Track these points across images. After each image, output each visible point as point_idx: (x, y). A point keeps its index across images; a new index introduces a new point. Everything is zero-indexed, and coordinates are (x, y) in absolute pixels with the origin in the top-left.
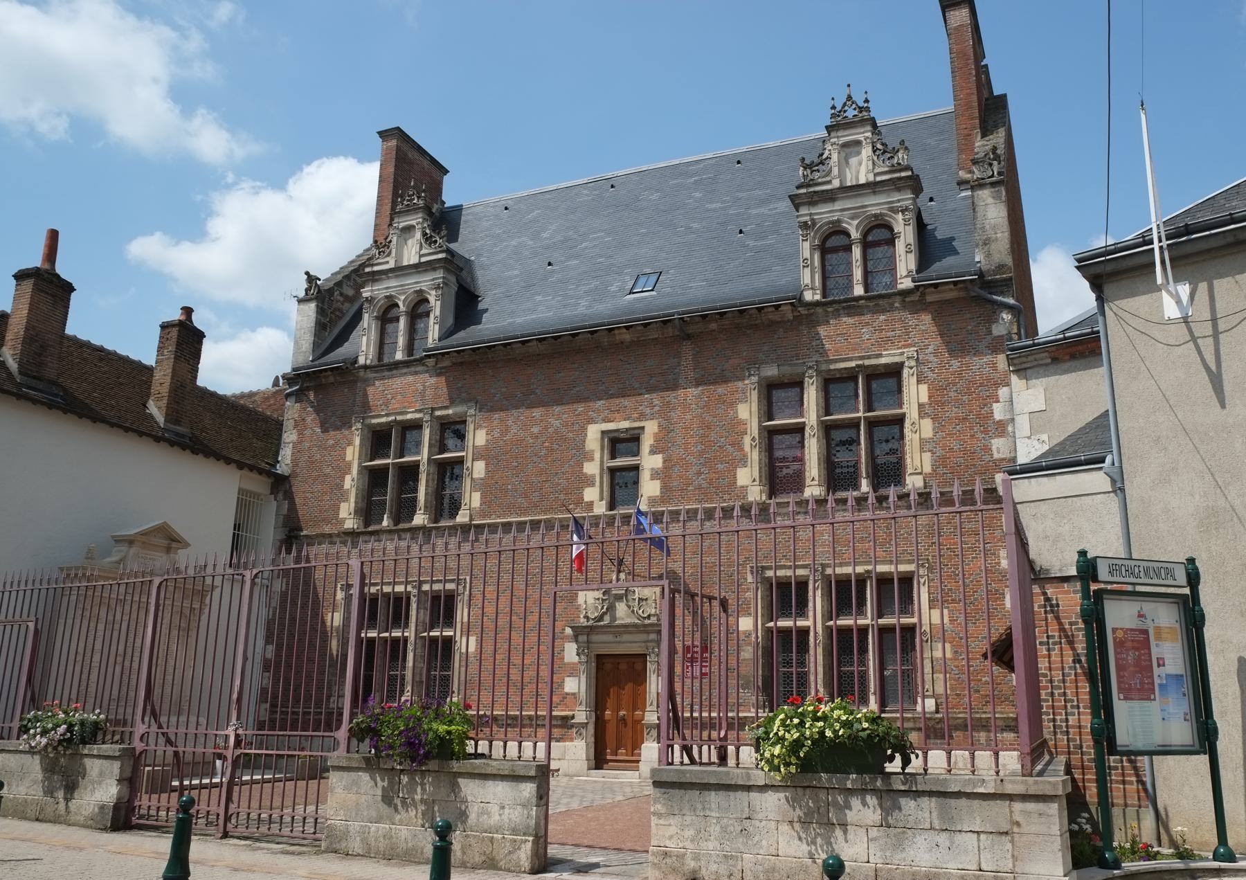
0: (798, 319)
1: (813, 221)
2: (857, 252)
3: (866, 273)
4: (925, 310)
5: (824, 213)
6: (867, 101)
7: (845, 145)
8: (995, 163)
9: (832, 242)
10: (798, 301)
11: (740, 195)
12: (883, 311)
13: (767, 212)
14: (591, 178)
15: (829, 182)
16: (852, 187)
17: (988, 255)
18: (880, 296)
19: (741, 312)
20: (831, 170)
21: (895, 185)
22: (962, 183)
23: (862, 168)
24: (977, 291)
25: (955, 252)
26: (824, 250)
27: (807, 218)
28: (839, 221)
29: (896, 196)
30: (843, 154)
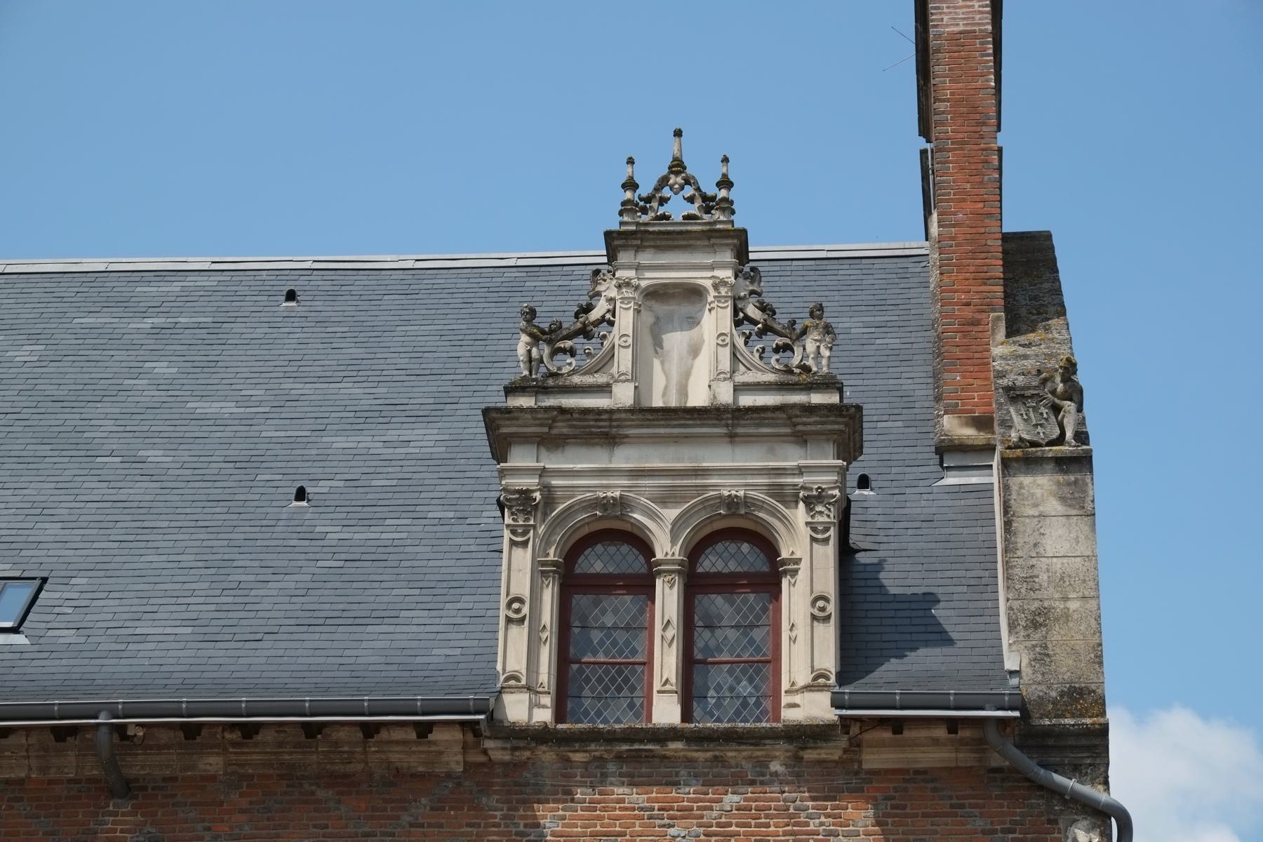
0: (480, 774)
1: (547, 490)
2: (668, 599)
3: (689, 663)
4: (856, 792)
5: (583, 474)
6: (725, 183)
7: (656, 294)
8: (1069, 406)
9: (596, 562)
10: (483, 723)
11: (298, 388)
12: (736, 781)
13: (377, 448)
14: (823, 248)
15: (605, 389)
16: (667, 414)
17: (1042, 657)
18: (731, 737)
19: (312, 731)
20: (611, 355)
21: (795, 425)
22: (947, 450)
23: (700, 363)
24: (1006, 754)
25: (941, 637)
26: (572, 582)
27: (530, 482)
28: (622, 504)
29: (792, 457)
30: (648, 318)
